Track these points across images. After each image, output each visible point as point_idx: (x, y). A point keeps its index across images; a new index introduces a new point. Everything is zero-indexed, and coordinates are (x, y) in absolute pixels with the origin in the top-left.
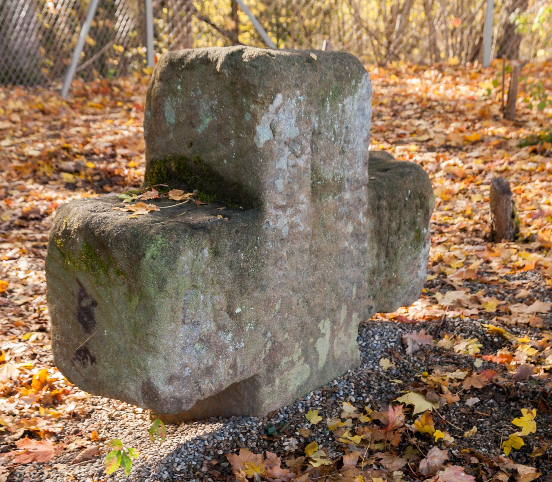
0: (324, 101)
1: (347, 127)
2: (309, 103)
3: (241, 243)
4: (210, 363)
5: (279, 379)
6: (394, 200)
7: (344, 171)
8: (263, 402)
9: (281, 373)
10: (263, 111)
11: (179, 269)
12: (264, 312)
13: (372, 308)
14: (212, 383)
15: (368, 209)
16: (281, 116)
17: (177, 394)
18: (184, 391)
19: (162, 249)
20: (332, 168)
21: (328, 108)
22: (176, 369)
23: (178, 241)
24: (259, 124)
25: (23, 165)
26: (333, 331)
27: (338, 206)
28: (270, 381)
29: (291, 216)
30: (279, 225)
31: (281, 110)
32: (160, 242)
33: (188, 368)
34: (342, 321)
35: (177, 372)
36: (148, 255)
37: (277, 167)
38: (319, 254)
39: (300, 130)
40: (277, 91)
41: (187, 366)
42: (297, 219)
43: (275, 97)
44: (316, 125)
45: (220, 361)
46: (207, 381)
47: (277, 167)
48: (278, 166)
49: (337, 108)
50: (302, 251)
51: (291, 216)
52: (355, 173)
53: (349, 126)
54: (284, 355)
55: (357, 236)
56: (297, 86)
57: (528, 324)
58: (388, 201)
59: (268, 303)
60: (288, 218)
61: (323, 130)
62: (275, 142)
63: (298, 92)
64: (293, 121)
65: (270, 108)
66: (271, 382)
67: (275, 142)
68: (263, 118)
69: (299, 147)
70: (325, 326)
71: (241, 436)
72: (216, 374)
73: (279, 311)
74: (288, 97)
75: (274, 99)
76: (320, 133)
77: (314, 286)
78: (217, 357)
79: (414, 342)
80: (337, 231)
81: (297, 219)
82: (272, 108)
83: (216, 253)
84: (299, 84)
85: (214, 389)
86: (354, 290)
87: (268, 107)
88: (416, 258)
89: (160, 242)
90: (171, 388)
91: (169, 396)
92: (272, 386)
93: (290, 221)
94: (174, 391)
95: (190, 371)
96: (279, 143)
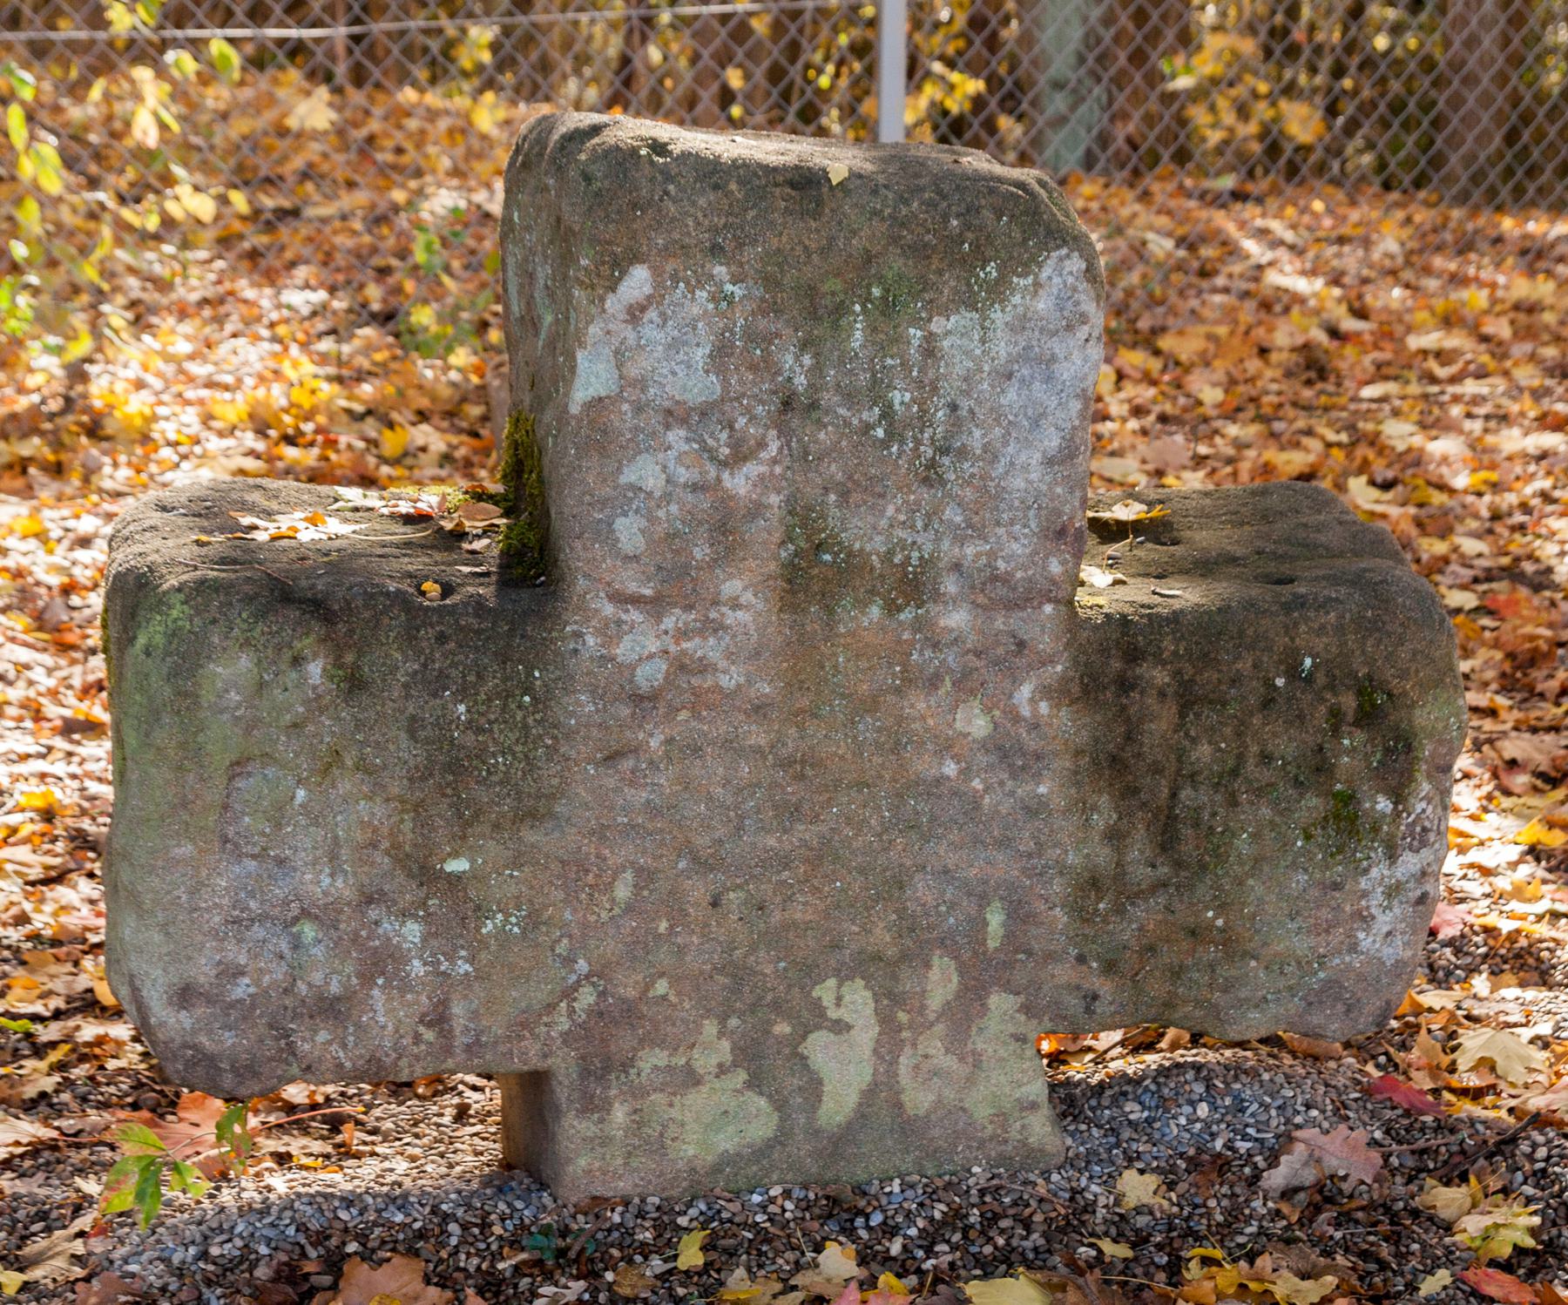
0: (840, 310)
1: (954, 407)
2: (771, 308)
3: (454, 673)
4: (335, 988)
5: (626, 1108)
6: (1210, 675)
7: (937, 540)
8: (569, 1161)
9: (639, 1093)
10: (594, 310)
11: (207, 697)
12: (561, 895)
13: (1095, 997)
14: (344, 1046)
15: (1064, 680)
16: (650, 332)
17: (203, 1039)
18: (229, 1039)
19: (174, 634)
20: (884, 523)
21: (858, 334)
22: (203, 971)
23: (214, 621)
24: (582, 345)
25: (1218, 424)
26: (886, 1021)
27: (912, 643)
28: (593, 1106)
29: (683, 634)
30: (624, 650)
31: (652, 314)
32: (175, 613)
33: (247, 980)
34: (935, 1002)
35: (202, 979)
36: (142, 640)
37: (623, 480)
38: (809, 772)
39: (725, 383)
40: (636, 258)
41: (243, 974)
42: (709, 648)
43: (623, 273)
44: (801, 381)
45: (376, 992)
46: (323, 1036)
47: (623, 480)
48: (629, 476)
49: (899, 340)
50: (731, 746)
51: (683, 634)
52: (992, 555)
53: (965, 404)
54: (652, 1040)
55: (1007, 752)
56: (716, 251)
57: (218, 1126)
58: (1177, 673)
59: (580, 875)
60: (668, 639)
61: (828, 398)
62: (626, 407)
63: (720, 271)
64: (700, 354)
65: (608, 304)
66: (597, 1109)
67: (626, 407)
68: (592, 330)
69: (724, 436)
70: (856, 1003)
71: (453, 1228)
72: (358, 1026)
73: (629, 909)
74: (676, 279)
75: (620, 279)
76: (814, 405)
77: (786, 866)
78: (367, 980)
79: (1314, 1159)
80: (900, 720)
81: (709, 648)
82: (613, 304)
83: (353, 684)
84: (729, 246)
85: (348, 1064)
86: (995, 920)
87: (602, 300)
88: (1337, 887)
89: (175, 613)
90: (185, 1019)
91: (178, 1040)
92: (601, 1121)
93: (672, 648)
94: (194, 1032)
95: (252, 990)
96: (639, 409)
